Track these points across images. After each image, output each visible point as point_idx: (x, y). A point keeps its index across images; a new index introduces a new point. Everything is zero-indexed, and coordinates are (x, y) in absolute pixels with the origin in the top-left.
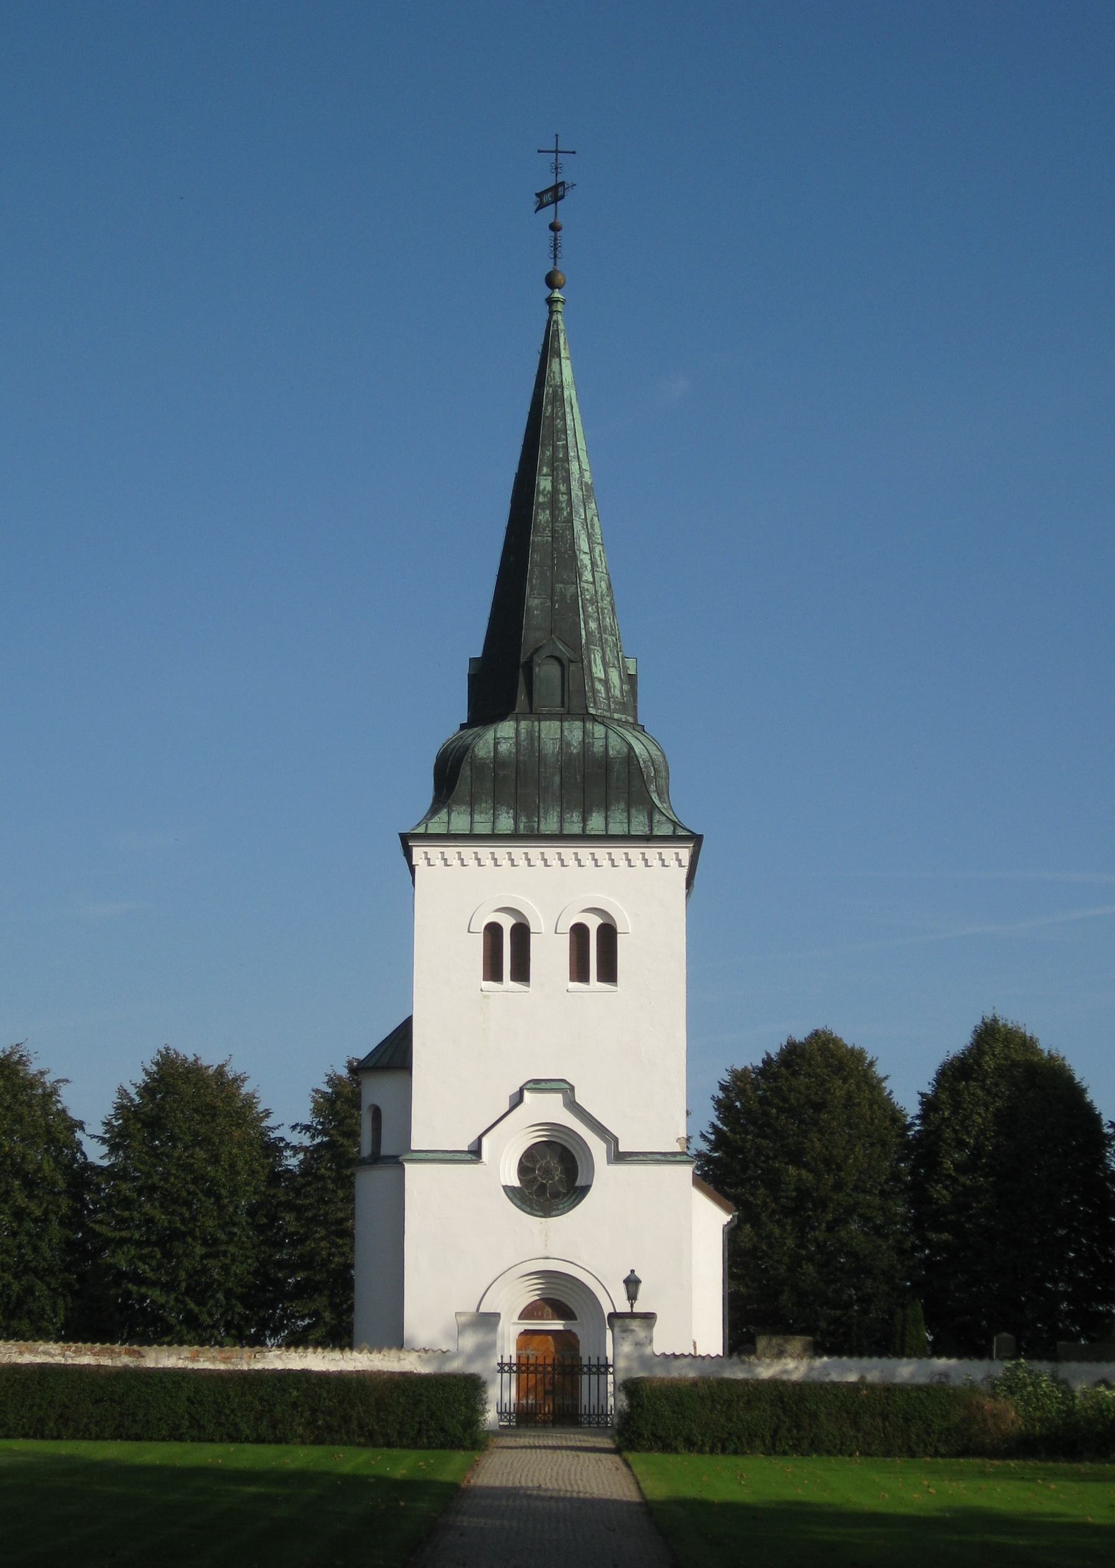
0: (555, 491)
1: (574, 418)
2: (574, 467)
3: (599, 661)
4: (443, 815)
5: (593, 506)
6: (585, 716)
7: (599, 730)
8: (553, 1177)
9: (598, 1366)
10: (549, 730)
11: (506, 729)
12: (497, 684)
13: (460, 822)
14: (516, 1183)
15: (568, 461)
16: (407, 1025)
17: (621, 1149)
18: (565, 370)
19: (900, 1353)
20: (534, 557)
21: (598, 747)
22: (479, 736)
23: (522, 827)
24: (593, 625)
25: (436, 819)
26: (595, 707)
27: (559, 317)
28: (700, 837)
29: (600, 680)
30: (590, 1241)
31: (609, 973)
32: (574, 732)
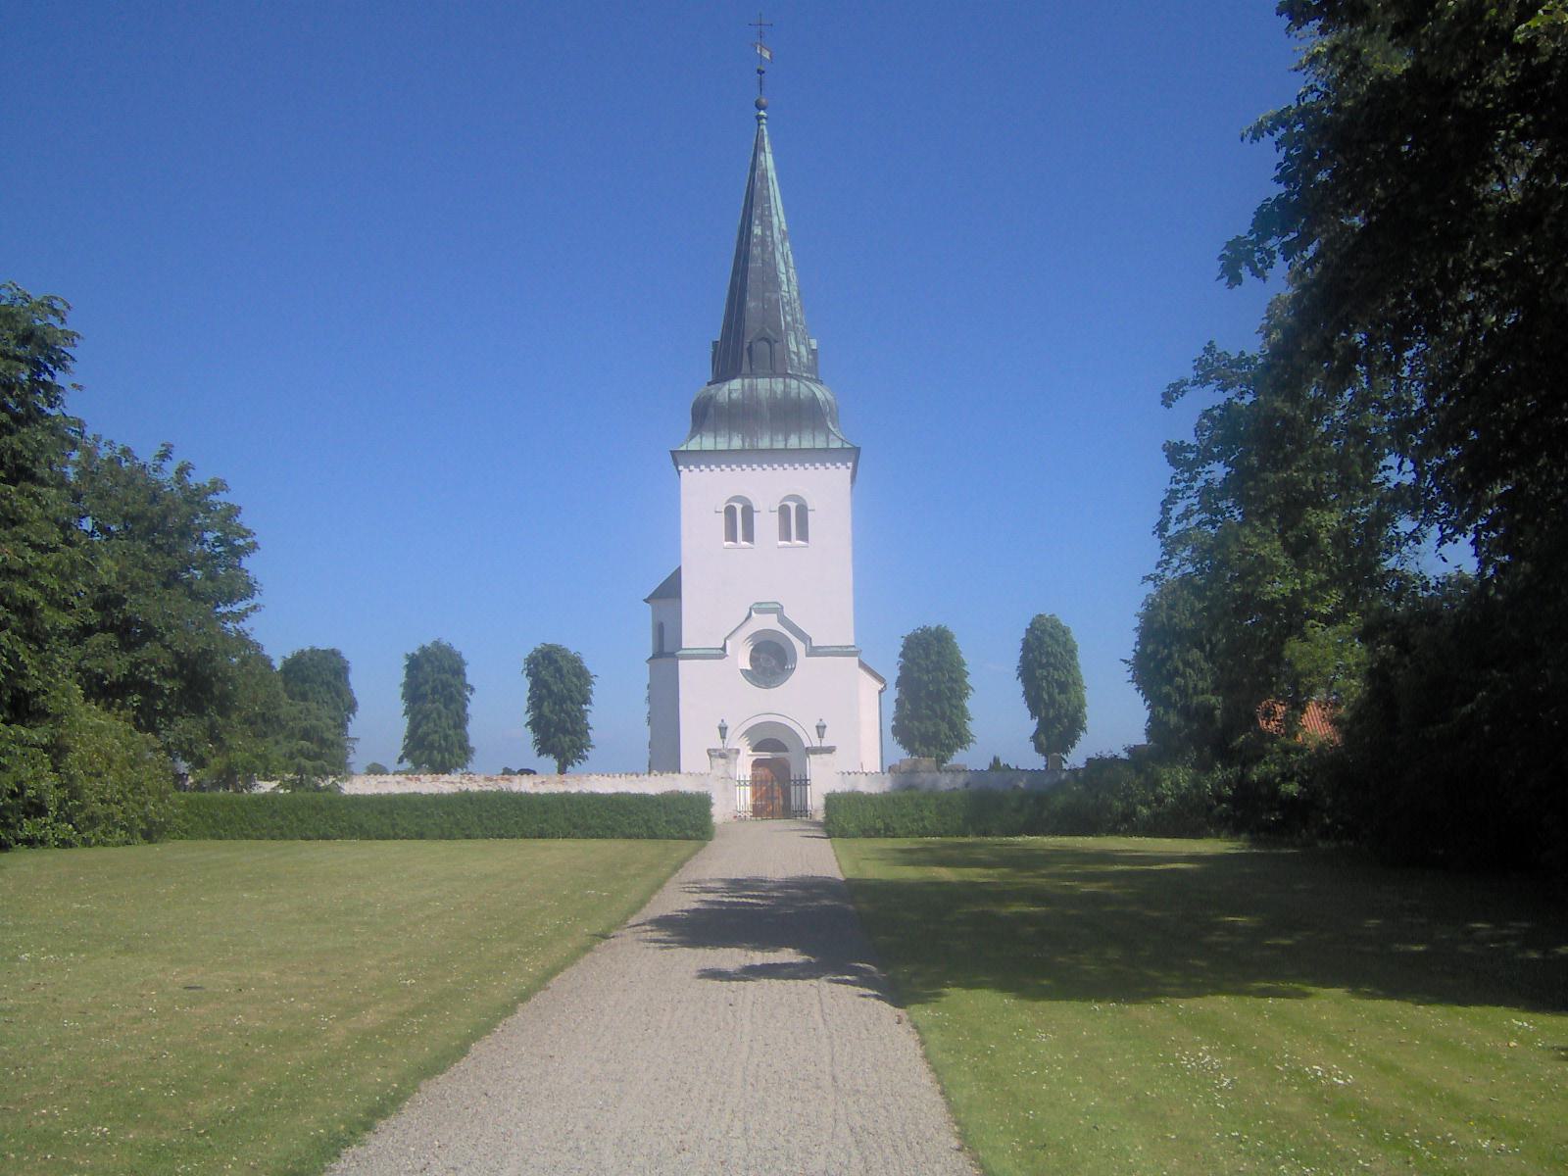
0: (764, 234)
1: (775, 190)
2: (775, 220)
3: (793, 341)
4: (697, 438)
5: (788, 244)
6: (785, 375)
7: (794, 383)
8: (771, 660)
9: (800, 781)
10: (763, 384)
11: (736, 384)
12: (730, 358)
13: (707, 443)
14: (749, 668)
15: (771, 216)
16: (680, 568)
17: (814, 645)
18: (768, 160)
19: (989, 836)
20: (751, 276)
21: (793, 394)
22: (720, 389)
23: (747, 444)
24: (789, 318)
25: (693, 441)
26: (792, 369)
27: (764, 127)
28: (859, 449)
29: (794, 353)
30: (791, 704)
31: (803, 535)
32: (778, 385)
